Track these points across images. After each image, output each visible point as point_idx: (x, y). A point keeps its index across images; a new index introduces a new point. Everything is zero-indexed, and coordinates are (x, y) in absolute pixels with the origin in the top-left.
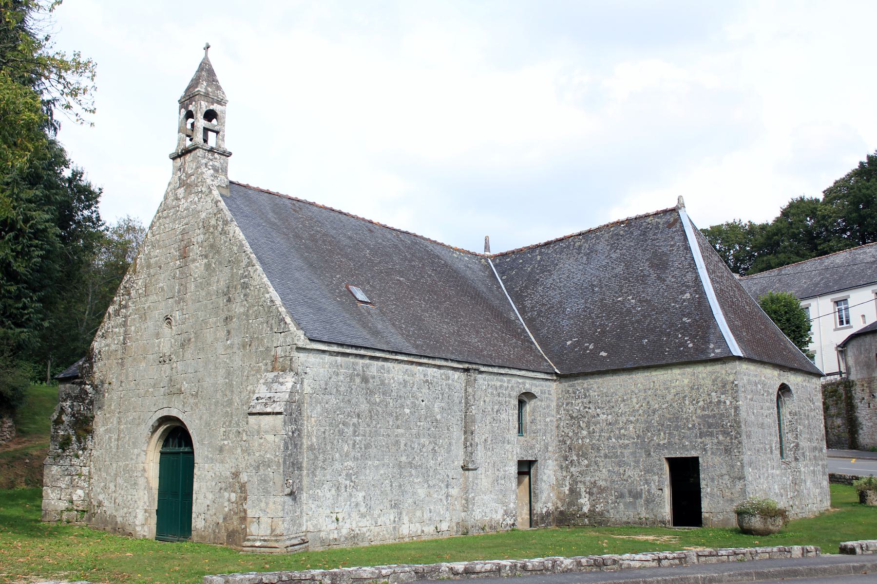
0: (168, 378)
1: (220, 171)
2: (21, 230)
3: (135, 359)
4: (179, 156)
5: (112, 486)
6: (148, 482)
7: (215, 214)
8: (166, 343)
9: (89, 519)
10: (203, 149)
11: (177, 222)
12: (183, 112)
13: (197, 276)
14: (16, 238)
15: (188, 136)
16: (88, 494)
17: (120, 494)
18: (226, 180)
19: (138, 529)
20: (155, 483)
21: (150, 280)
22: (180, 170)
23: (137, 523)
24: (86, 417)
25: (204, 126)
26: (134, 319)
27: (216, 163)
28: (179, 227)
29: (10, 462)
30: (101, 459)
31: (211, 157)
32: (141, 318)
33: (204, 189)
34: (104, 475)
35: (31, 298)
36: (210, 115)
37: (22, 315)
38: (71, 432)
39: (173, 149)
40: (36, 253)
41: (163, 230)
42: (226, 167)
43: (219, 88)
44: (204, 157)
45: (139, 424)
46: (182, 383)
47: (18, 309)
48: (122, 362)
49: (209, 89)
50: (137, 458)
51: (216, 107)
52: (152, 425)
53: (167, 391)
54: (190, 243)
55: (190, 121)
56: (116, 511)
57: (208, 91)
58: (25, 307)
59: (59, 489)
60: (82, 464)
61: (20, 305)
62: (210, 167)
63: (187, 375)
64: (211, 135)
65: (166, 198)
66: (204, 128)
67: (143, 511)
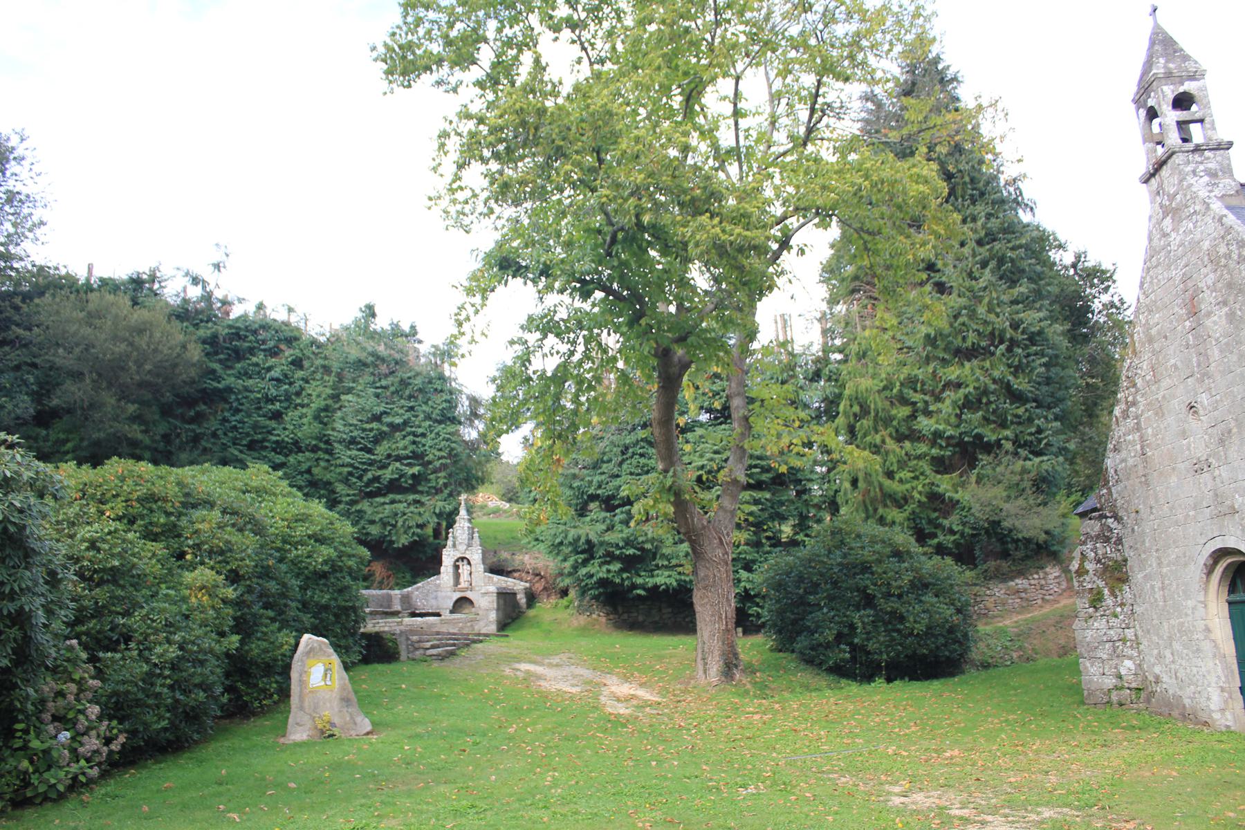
0: (1211, 493)
1: (1220, 173)
2: (1011, 340)
3: (1161, 473)
4: (1153, 175)
5: (1168, 655)
6: (1216, 646)
7: (1223, 237)
8: (1198, 445)
9: (1148, 701)
10: (1183, 152)
11: (1172, 267)
12: (1143, 112)
13: (1218, 335)
14: (1009, 349)
15: (1158, 143)
16: (1140, 665)
17: (1181, 665)
18: (1233, 184)
19: (1216, 716)
20: (1229, 648)
21: (1157, 359)
22: (1158, 193)
23: (1212, 707)
24: (1116, 561)
25: (1176, 119)
26: (1148, 418)
27: (1210, 165)
28: (1176, 273)
29: (1057, 622)
30: (1146, 616)
31: (1199, 159)
32: (1157, 414)
33: (1197, 208)
34: (1155, 638)
35: (1046, 418)
36: (1183, 101)
37: (1040, 441)
38: (1101, 584)
39: (1143, 167)
40: (1038, 362)
41: (1157, 285)
42: (1229, 165)
43: (1186, 58)
44: (1188, 162)
45: (1186, 565)
46: (1234, 496)
47: (1031, 434)
48: (1146, 480)
49: (1171, 65)
50: (1193, 613)
51: (1188, 86)
52: (1205, 564)
53: (1214, 512)
54: (1198, 291)
55: (1156, 121)
56: (1181, 689)
57: (1169, 69)
58: (1040, 431)
59: (1099, 661)
60: (1124, 626)
61: (1033, 430)
62: (1202, 174)
63: (1238, 484)
64: (1195, 129)
65: (1150, 240)
66: (1179, 123)
67: (1219, 691)
